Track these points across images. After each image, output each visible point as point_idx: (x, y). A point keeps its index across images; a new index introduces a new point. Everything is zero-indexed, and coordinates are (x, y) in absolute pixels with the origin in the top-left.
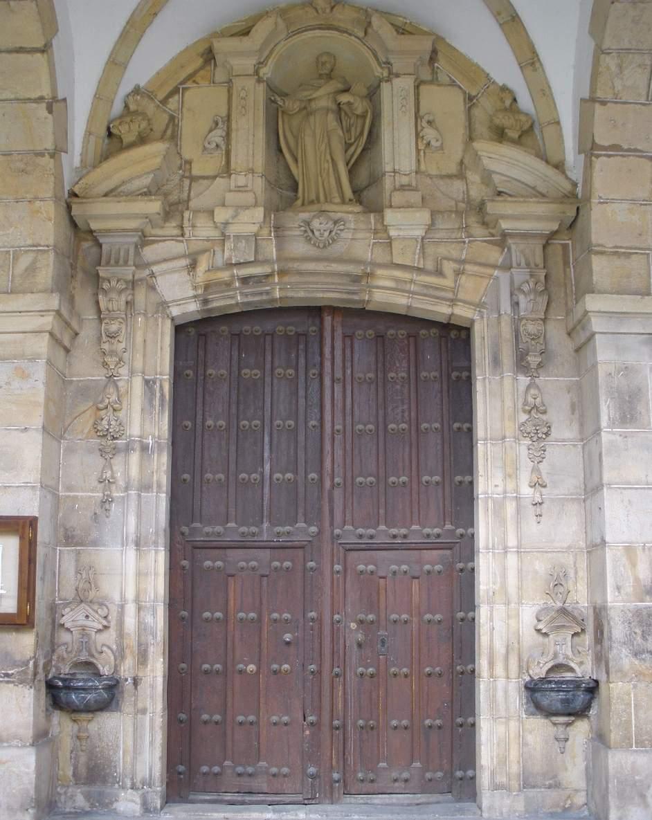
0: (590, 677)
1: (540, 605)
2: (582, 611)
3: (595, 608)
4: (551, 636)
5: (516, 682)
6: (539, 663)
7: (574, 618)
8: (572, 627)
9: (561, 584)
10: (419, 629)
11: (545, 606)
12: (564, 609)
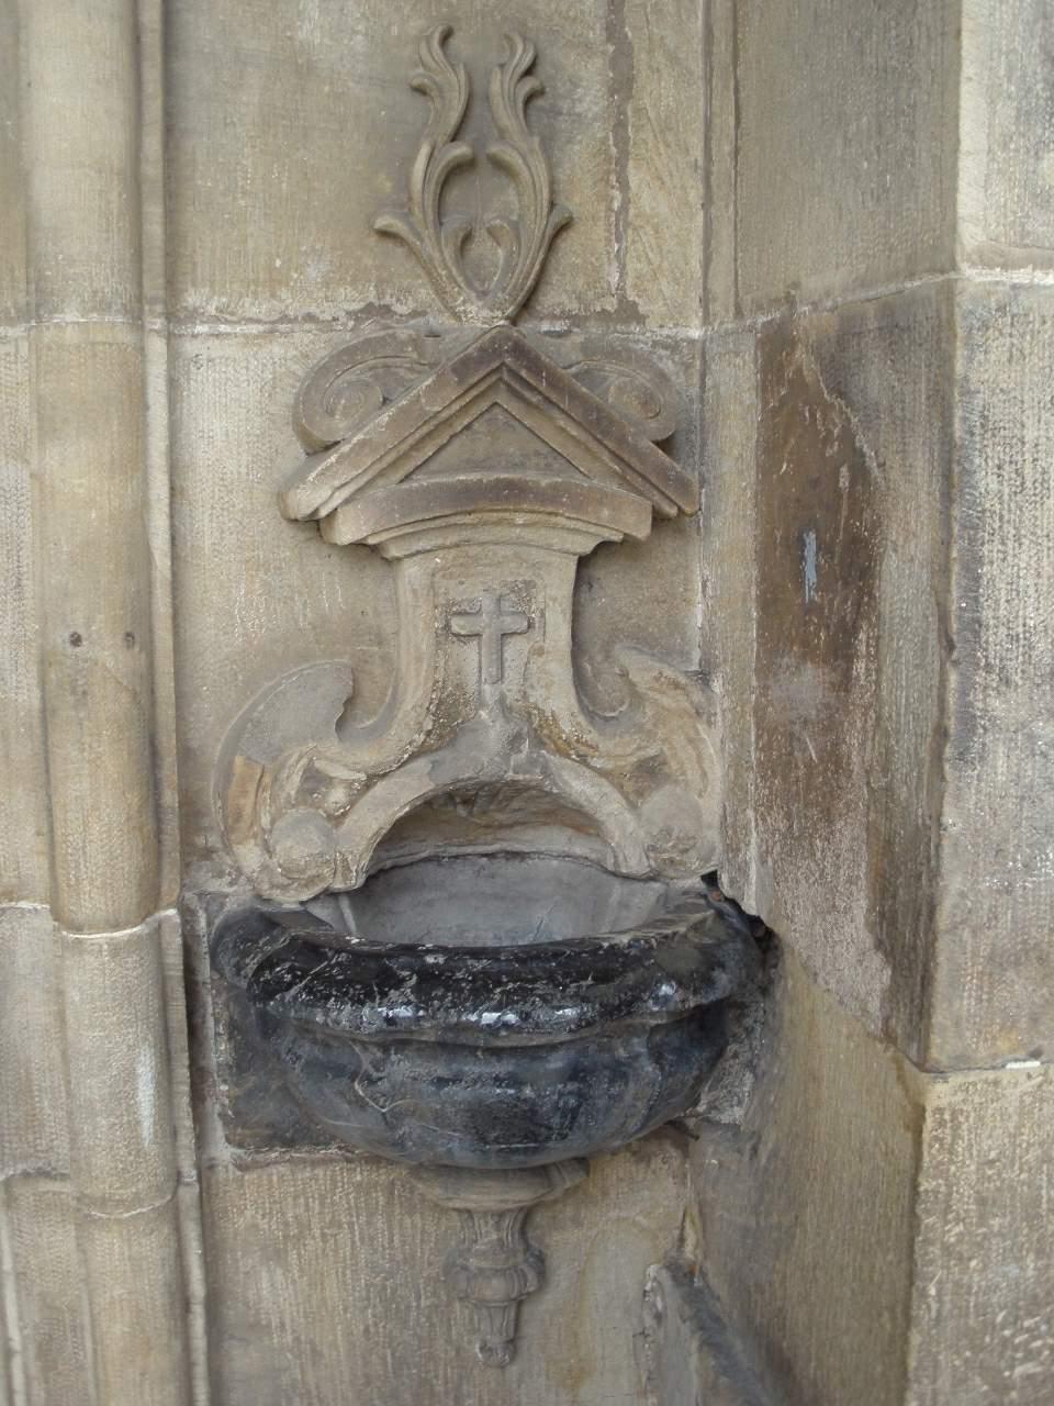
0: (711, 879)
1: (328, 326)
2: (662, 376)
3: (776, 346)
4: (412, 572)
5: (116, 950)
6: (315, 781)
7: (599, 424)
8: (580, 501)
9: (500, 166)
10: (387, 530)
11: (369, 329)
12: (519, 350)
